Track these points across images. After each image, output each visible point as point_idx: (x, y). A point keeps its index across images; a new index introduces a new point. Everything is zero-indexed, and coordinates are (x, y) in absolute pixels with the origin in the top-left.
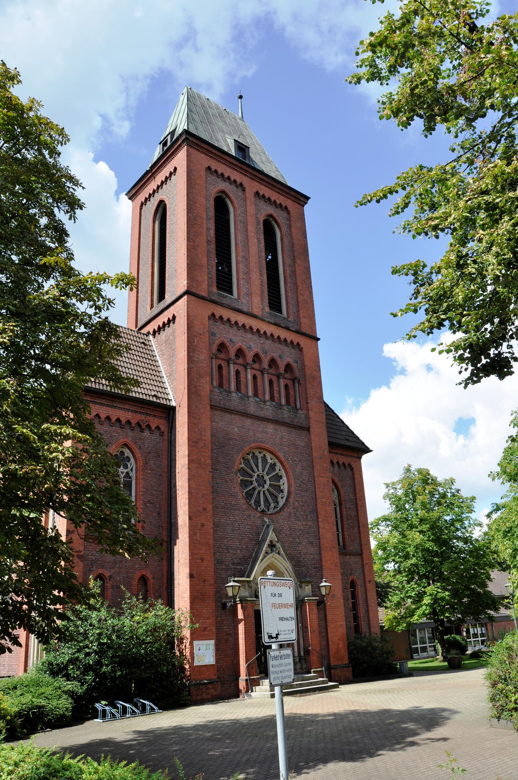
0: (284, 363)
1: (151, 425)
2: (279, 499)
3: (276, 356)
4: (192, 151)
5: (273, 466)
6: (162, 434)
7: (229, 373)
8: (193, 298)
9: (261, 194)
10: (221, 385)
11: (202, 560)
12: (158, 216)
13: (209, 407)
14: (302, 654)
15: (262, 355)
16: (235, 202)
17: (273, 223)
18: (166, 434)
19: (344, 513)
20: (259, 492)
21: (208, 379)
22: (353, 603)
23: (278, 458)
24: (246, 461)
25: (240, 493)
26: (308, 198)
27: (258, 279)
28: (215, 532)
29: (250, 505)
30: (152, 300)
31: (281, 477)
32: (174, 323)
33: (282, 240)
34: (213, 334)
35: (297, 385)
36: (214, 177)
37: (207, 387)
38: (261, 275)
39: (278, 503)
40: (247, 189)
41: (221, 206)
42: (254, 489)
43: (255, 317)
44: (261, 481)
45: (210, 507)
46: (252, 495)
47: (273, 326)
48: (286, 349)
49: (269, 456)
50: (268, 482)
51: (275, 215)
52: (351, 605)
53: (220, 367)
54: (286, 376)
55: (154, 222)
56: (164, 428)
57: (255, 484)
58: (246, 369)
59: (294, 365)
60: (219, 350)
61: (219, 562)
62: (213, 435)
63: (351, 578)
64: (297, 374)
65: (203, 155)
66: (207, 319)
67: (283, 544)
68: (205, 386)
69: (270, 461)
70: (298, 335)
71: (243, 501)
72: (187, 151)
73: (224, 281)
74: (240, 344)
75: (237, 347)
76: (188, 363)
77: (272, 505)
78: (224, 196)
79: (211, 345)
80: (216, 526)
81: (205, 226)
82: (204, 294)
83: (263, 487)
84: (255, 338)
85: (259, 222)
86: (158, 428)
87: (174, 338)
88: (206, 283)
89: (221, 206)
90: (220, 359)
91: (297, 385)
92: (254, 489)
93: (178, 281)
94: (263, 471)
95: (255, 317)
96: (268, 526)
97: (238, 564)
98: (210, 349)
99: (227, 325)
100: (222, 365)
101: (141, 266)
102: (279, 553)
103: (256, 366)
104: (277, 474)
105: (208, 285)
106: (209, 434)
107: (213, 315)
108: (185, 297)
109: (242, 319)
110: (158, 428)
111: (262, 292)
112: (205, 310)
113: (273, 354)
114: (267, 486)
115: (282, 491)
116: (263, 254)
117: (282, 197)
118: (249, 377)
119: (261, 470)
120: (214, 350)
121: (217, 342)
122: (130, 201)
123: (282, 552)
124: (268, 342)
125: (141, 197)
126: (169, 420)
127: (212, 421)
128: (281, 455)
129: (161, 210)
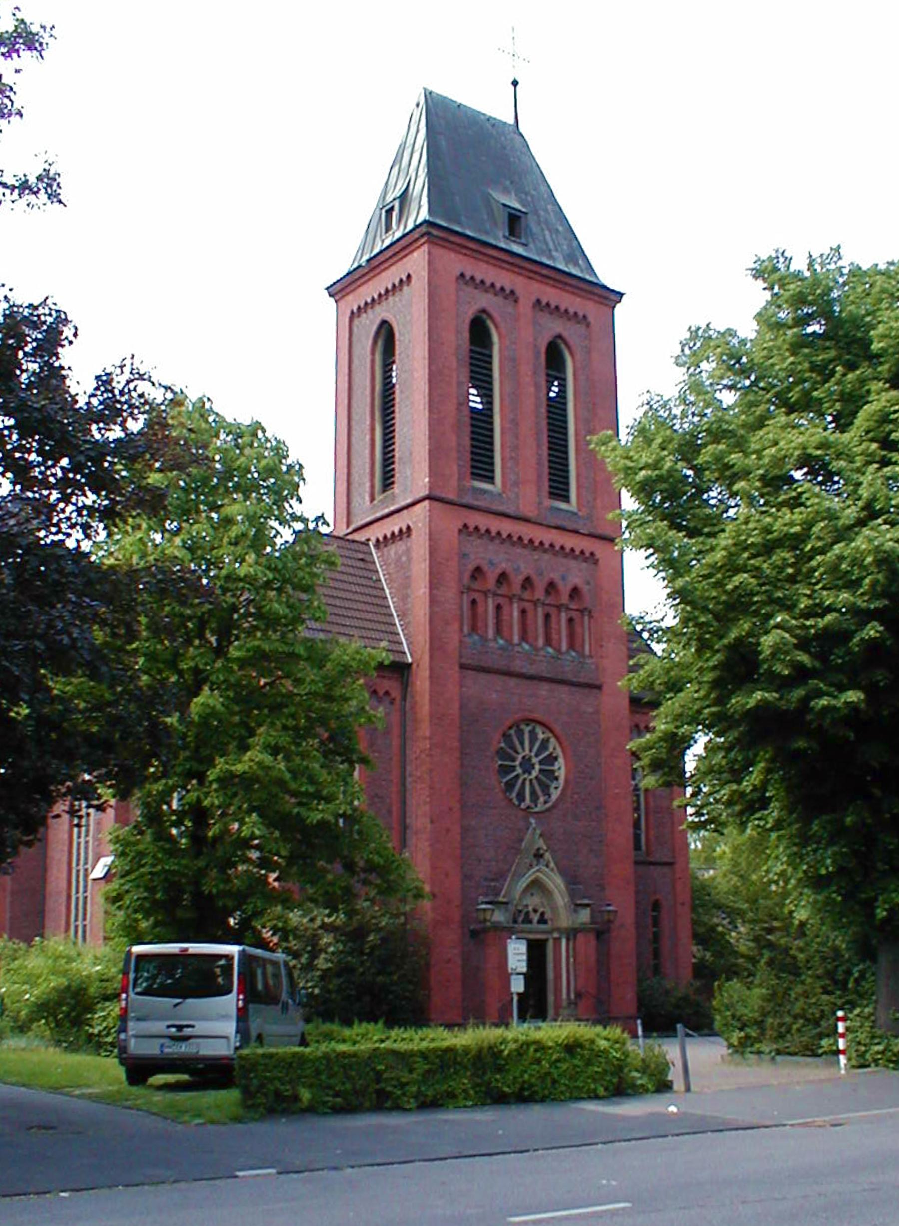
0: (569, 587)
1: (378, 690)
2: (552, 790)
3: (556, 576)
4: (438, 251)
5: (545, 744)
6: (392, 702)
7: (486, 611)
8: (436, 504)
9: (544, 302)
10: (474, 629)
11: (446, 875)
12: (380, 343)
13: (457, 668)
14: (573, 996)
15: (535, 577)
16: (502, 325)
17: (563, 346)
18: (398, 702)
19: (652, 804)
20: (525, 780)
21: (456, 626)
22: (655, 933)
23: (551, 731)
24: (506, 736)
25: (497, 783)
26: (621, 295)
27: (535, 452)
28: (463, 839)
29: (511, 800)
30: (372, 486)
31: (556, 759)
32: (409, 536)
33: (575, 375)
34: (464, 555)
35: (586, 618)
36: (469, 289)
37: (456, 638)
38: (539, 446)
39: (550, 796)
40: (522, 300)
41: (479, 330)
42: (517, 776)
43: (527, 520)
44: (527, 766)
45: (457, 806)
46: (514, 786)
47: (554, 531)
48: (573, 563)
49: (539, 730)
50: (537, 767)
51: (565, 334)
52: (651, 936)
53: (474, 602)
54: (573, 606)
55: (373, 353)
56: (395, 694)
57: (519, 770)
58: (511, 603)
59: (585, 589)
60: (473, 577)
61: (467, 877)
62: (462, 707)
63: (653, 898)
64: (588, 601)
65: (453, 255)
66: (456, 534)
67: (554, 852)
68: (452, 637)
69: (541, 736)
70: (593, 539)
71: (501, 795)
72: (429, 253)
73: (481, 465)
74: (504, 565)
75: (499, 571)
76: (431, 606)
77: (542, 800)
78: (485, 316)
79: (461, 573)
80: (466, 831)
81: (455, 381)
82: (452, 496)
83: (530, 774)
84: (526, 552)
85: (539, 352)
86: (387, 693)
87: (409, 559)
88: (456, 476)
89: (479, 330)
90: (475, 590)
91: (586, 618)
92: (517, 776)
93: (414, 476)
94: (531, 751)
95: (527, 520)
96: (535, 829)
97: (493, 880)
98: (460, 579)
99: (486, 540)
100: (478, 600)
101: (353, 423)
102: (547, 866)
103: (527, 595)
104: (551, 754)
105: (459, 479)
106: (457, 706)
107: (466, 526)
108: (426, 503)
109: (506, 527)
110: (387, 693)
111: (539, 476)
112: (452, 521)
113: (552, 575)
114: (535, 774)
115: (557, 779)
116: (544, 383)
117: (578, 299)
118: (516, 614)
119: (527, 751)
120: (466, 580)
121: (471, 567)
122: (332, 300)
123: (552, 865)
124: (546, 556)
125: (353, 301)
126: (402, 684)
127: (462, 687)
128: (557, 729)
129: (386, 336)
